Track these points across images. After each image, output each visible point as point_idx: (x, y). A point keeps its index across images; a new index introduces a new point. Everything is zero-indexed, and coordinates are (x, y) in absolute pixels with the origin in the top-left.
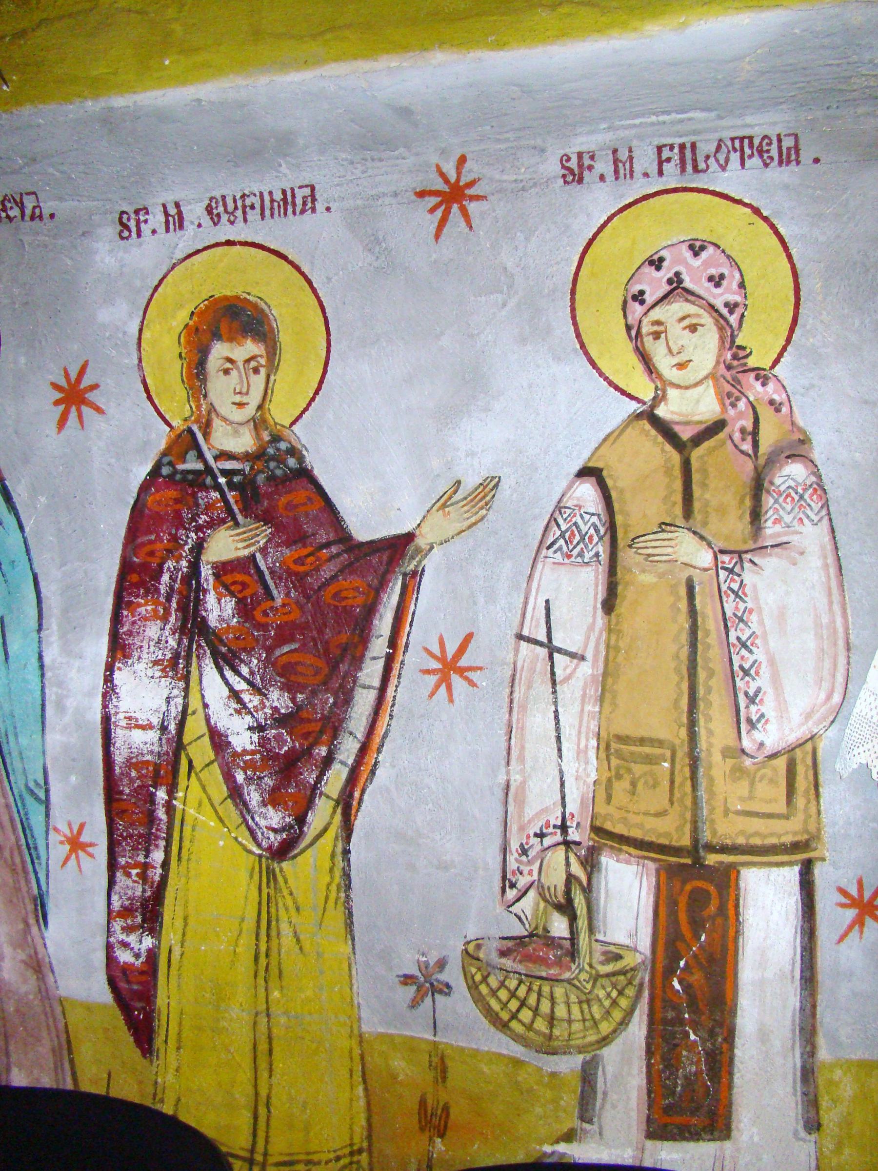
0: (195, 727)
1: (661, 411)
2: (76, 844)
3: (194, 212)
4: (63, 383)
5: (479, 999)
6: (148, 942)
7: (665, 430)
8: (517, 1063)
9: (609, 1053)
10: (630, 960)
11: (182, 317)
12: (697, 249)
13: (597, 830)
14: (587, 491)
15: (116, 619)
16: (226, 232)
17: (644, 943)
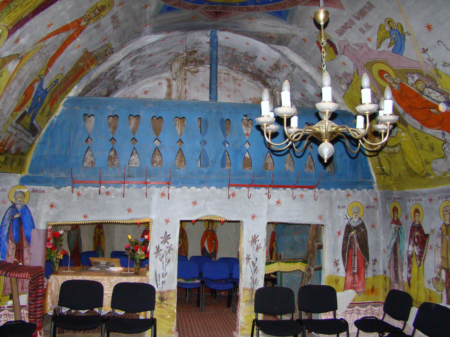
0: (414, 252)
1: (445, 223)
2: (406, 264)
3: (414, 200)
4: (431, 27)
5: (433, 284)
6: (410, 275)
7: (445, 224)
8: (436, 292)
9: (443, 292)
10: (444, 281)
11: (414, 210)
12: (326, 161)
13: (441, 266)
14: (440, 231)
15: (409, 240)
16: (416, 202)
17: (445, 280)
